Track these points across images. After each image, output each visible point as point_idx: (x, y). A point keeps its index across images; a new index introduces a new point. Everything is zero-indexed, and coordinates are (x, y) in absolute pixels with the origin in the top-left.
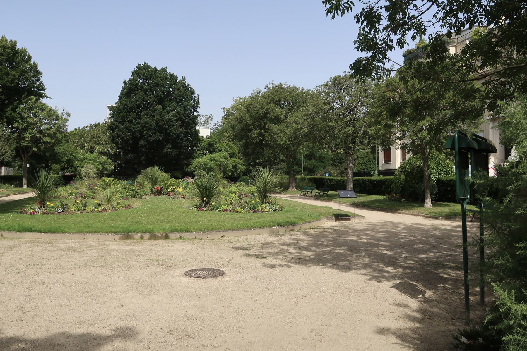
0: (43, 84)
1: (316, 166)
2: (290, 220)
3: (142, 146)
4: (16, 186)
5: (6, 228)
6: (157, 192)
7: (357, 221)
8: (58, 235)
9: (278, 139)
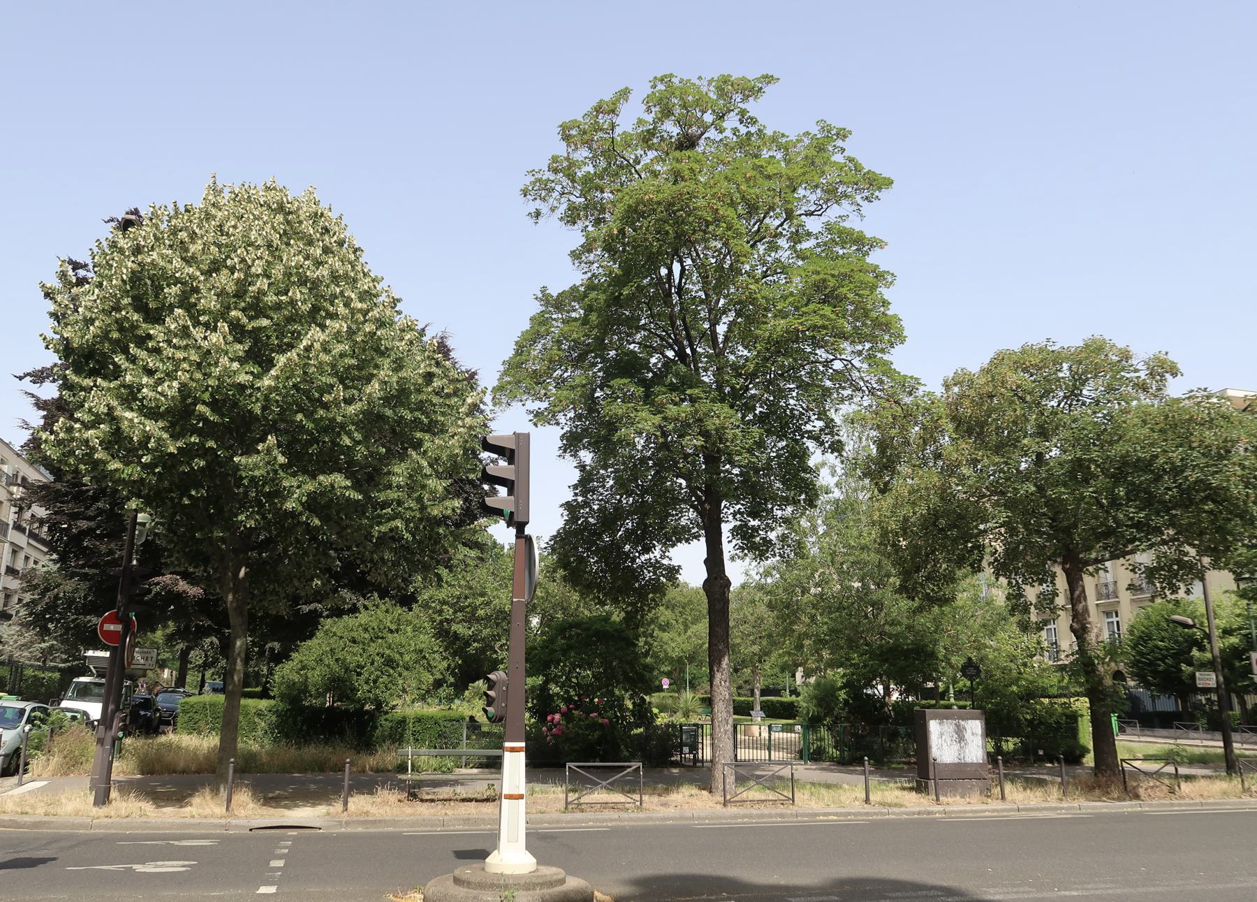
3: (887, 692)
9: (669, 650)
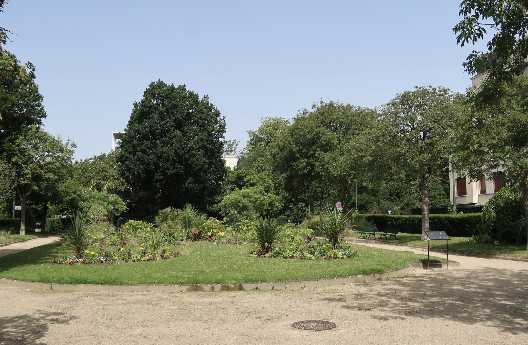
0: (43, 110)
1: (368, 201)
2: (374, 267)
3: (158, 181)
4: (13, 233)
5: (55, 279)
6: (195, 237)
7: (450, 268)
8: (117, 287)
9: (331, 169)
